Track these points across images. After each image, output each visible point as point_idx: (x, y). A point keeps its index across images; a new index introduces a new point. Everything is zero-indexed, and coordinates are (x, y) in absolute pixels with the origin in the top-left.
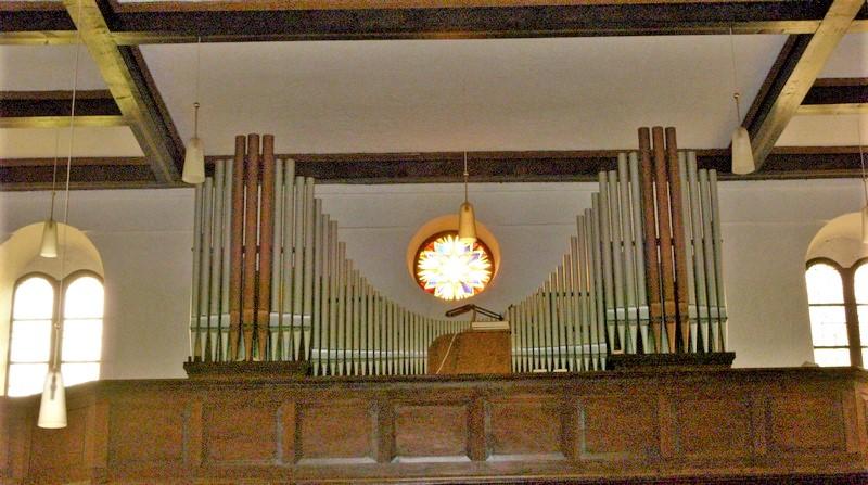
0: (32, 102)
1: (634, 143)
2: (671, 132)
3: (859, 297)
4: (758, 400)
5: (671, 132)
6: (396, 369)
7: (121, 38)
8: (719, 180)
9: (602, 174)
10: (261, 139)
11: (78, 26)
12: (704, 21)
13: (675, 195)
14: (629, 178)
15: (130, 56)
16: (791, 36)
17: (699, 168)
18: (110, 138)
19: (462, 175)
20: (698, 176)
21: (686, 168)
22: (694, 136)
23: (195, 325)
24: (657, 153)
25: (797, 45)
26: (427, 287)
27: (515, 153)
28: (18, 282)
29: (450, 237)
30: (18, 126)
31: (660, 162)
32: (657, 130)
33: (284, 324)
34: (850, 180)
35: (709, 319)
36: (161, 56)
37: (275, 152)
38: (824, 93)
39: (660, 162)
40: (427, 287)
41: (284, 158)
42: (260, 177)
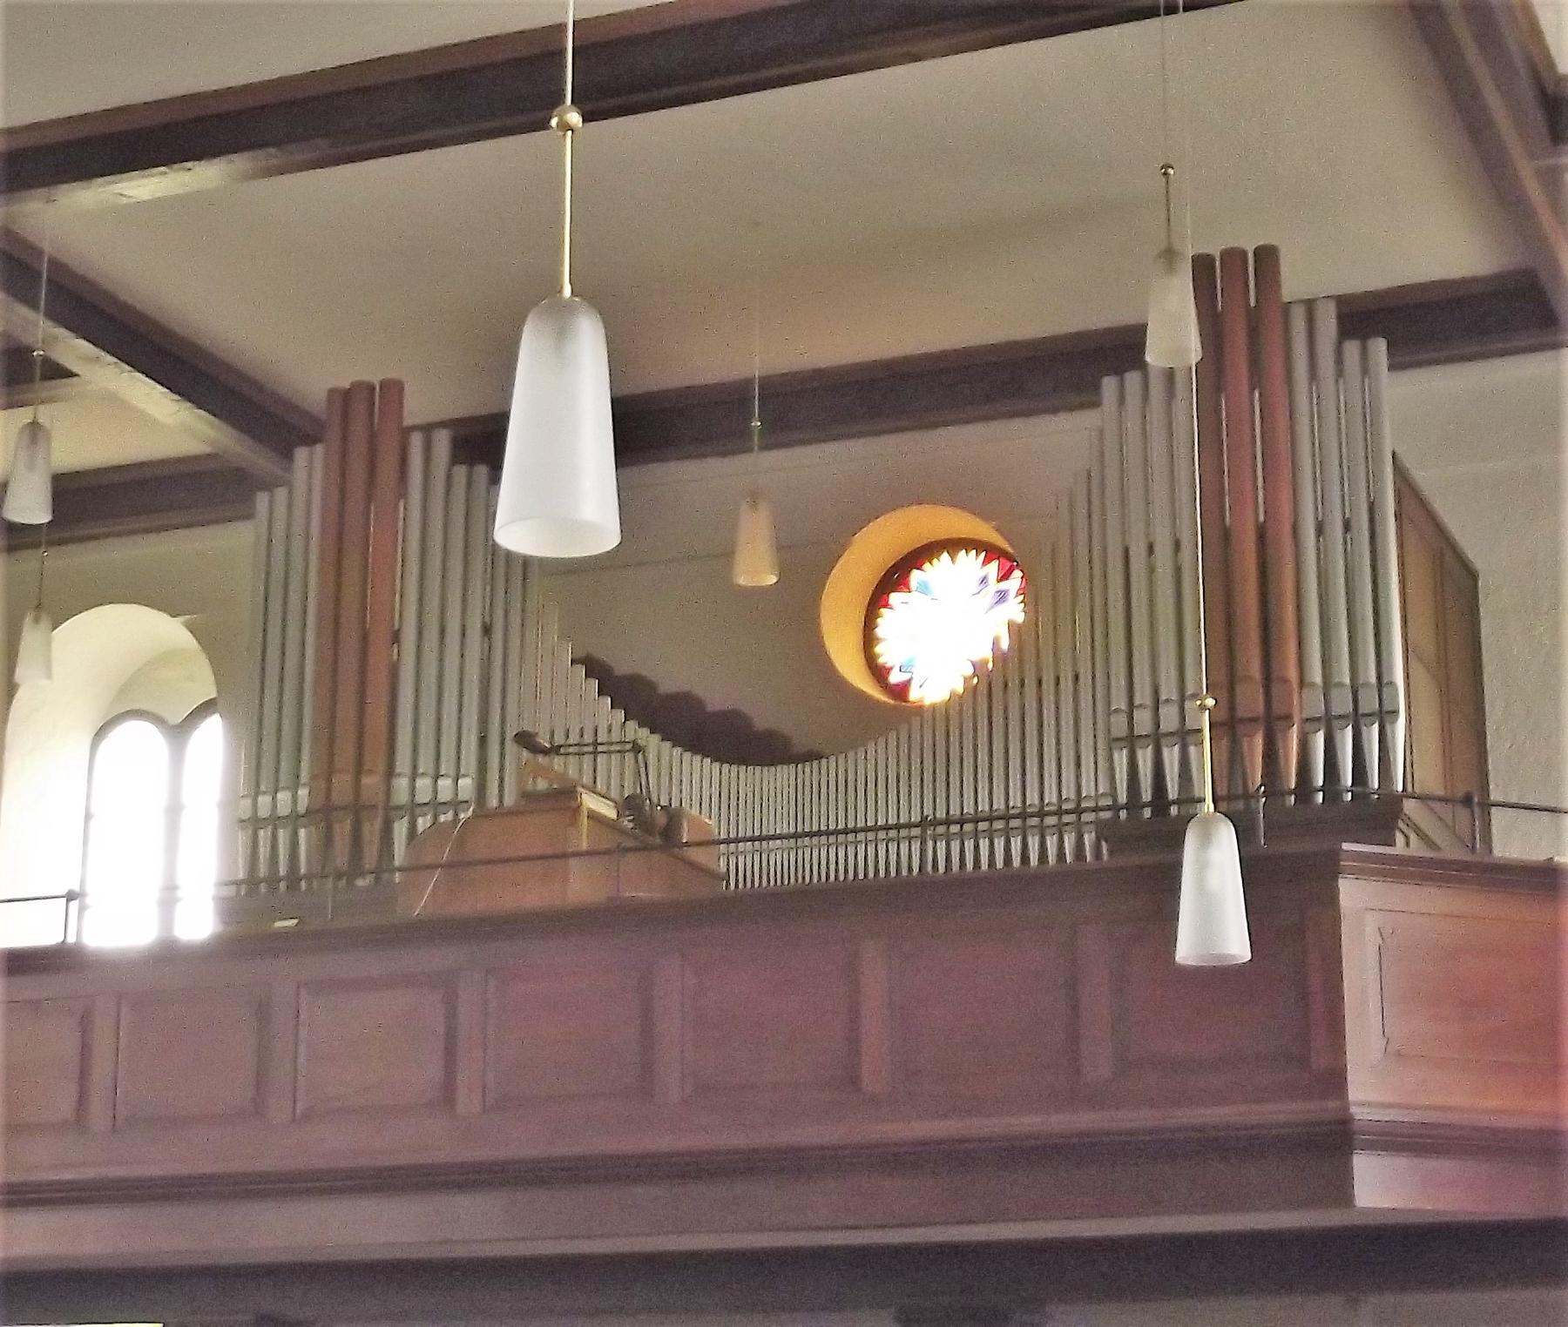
2: (1267, 257)
3: (186, 798)
4: (876, 973)
5: (1267, 257)
6: (841, 871)
9: (1109, 384)
17: (455, 459)
19: (745, 433)
23: (1279, 725)
26: (895, 678)
27: (943, 356)
28: (101, 733)
29: (945, 556)
32: (1234, 256)
33: (1336, 711)
34: (152, 537)
35: (1157, 739)
37: (408, 421)
40: (895, 678)
41: (428, 429)
42: (1257, 375)
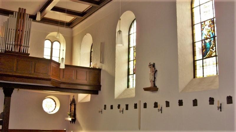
14: (15, 17)
22: (30, 11)
32: (22, 9)
38: (55, 9)
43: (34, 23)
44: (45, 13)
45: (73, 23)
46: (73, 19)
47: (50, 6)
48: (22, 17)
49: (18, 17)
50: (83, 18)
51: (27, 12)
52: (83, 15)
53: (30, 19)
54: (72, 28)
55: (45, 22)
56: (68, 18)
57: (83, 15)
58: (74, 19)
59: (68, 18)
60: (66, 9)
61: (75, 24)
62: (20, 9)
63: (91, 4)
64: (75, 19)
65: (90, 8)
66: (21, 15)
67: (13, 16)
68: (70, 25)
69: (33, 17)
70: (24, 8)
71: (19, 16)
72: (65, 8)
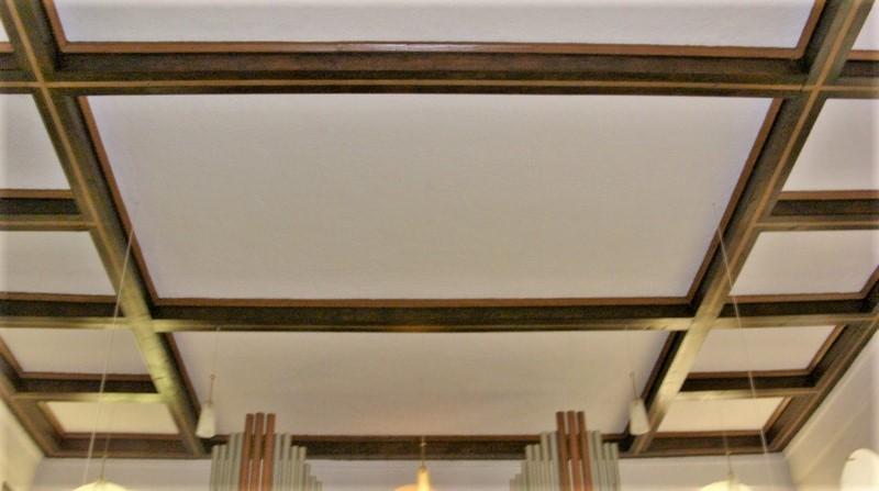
0: (618, 307)
1: (552, 427)
7: (163, 325)
8: (622, 458)
10: (265, 420)
11: (721, 320)
12: (295, 322)
13: (586, 467)
14: (550, 458)
15: (166, 340)
16: (672, 333)
18: (150, 414)
20: (603, 450)
21: (594, 448)
22: (600, 421)
24: (571, 437)
25: (676, 339)
27: (463, 437)
30: (89, 401)
31: (574, 442)
32: (571, 414)
36: (199, 344)
38: (694, 383)
39: (574, 442)
42: (262, 454)
43: (627, 466)
44: (658, 411)
45: (782, 426)
46: (779, 406)
47: (674, 372)
48: (575, 449)
49: (560, 455)
50: (816, 392)
51: (279, 429)
52: (815, 378)
53: (295, 448)
54: (781, 449)
55: (668, 453)
56: (754, 412)
57: (815, 378)
58: (782, 408)
59: (754, 412)
60: (746, 372)
61: (783, 439)
62: (560, 415)
63: (829, 315)
64: (785, 405)
65: (837, 334)
66: (568, 442)
67: (227, 452)
68: (772, 438)
69: (624, 442)
70: (577, 410)
71: (564, 453)
72: (99, 372)
